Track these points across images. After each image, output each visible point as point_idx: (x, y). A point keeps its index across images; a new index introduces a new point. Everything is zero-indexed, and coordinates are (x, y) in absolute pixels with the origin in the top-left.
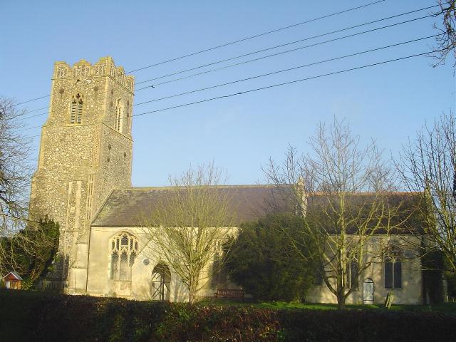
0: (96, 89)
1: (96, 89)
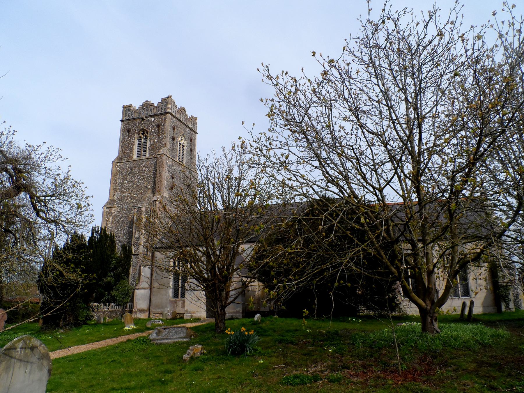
0: (158, 126)
1: (158, 126)
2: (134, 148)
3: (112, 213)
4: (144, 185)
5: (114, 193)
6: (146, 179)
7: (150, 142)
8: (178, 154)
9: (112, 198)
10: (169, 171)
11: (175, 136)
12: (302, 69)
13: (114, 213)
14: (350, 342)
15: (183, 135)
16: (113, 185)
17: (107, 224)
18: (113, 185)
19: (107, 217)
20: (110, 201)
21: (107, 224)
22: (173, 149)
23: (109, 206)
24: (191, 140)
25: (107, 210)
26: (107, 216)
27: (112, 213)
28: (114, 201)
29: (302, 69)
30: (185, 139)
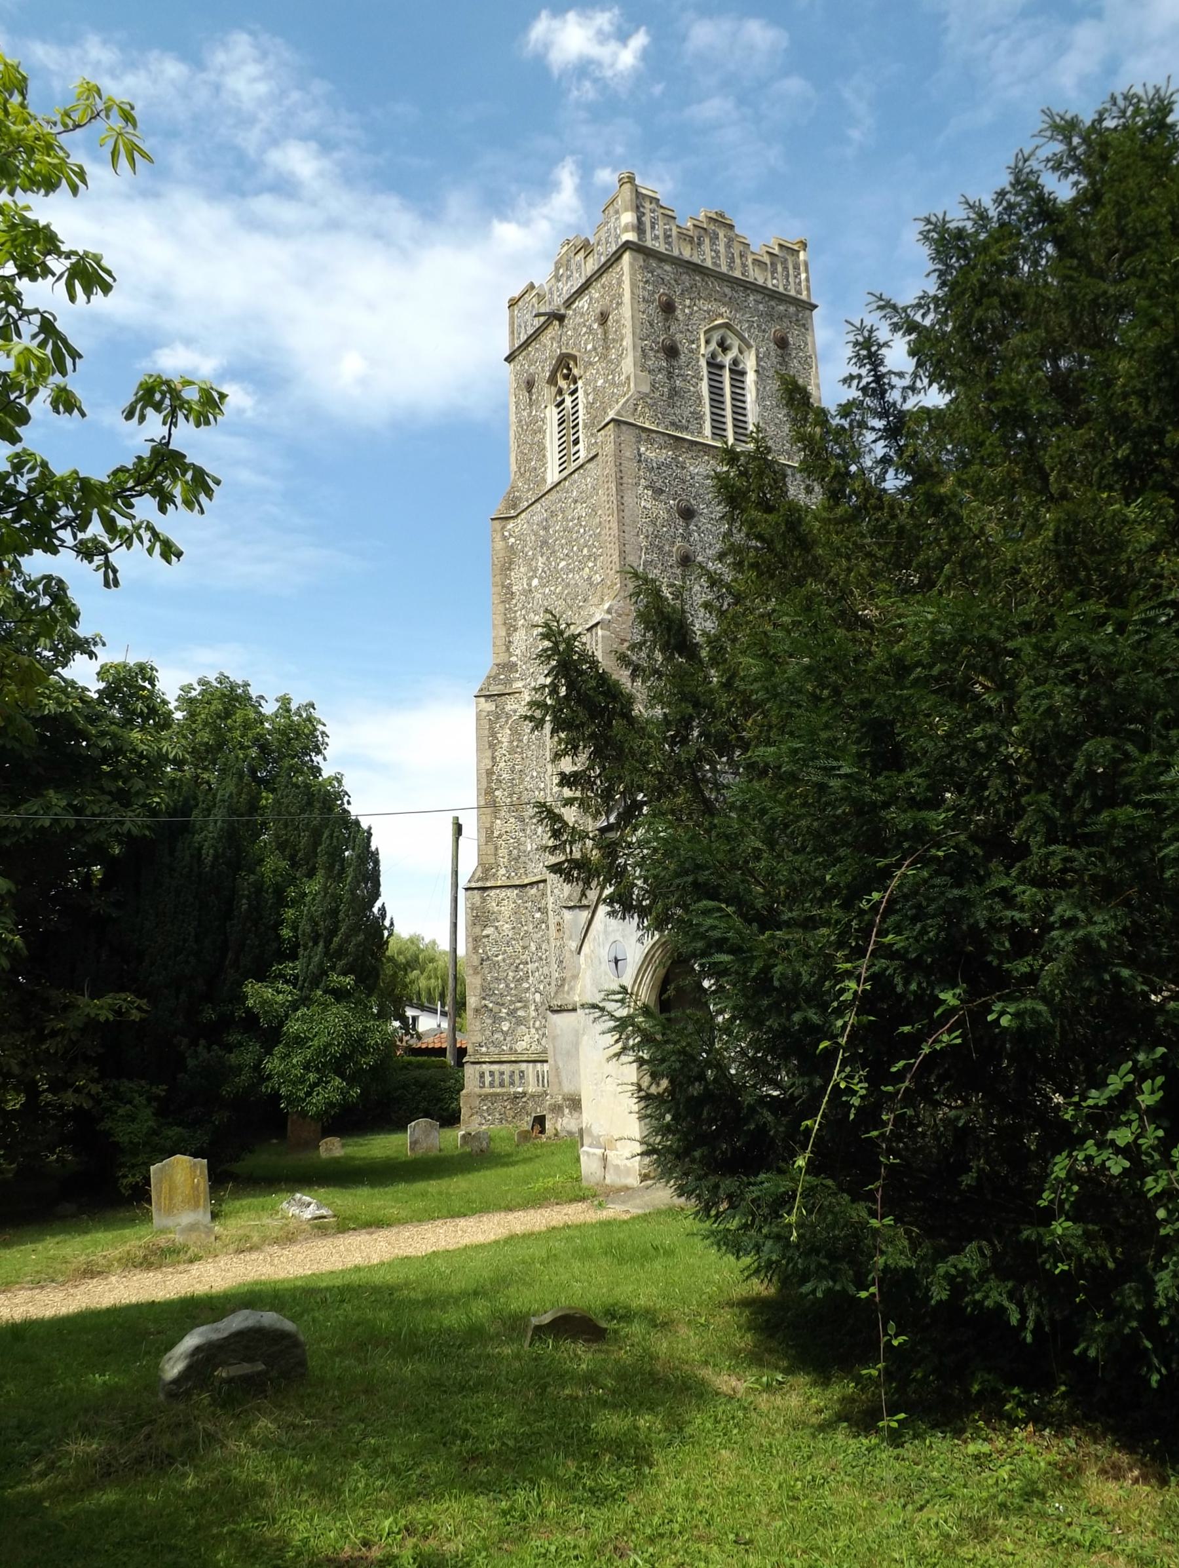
2: (548, 445)
3: (508, 717)
4: (581, 577)
5: (509, 635)
6: (585, 551)
7: (587, 394)
8: (707, 409)
9: (502, 658)
10: (658, 492)
11: (678, 336)
12: (1169, 77)
13: (515, 711)
14: (1054, 331)
15: (726, 326)
16: (501, 608)
17: (494, 758)
18: (501, 608)
19: (494, 734)
20: (495, 670)
21: (494, 758)
22: (674, 392)
23: (495, 690)
24: (782, 343)
25: (489, 706)
26: (491, 728)
27: (508, 717)
28: (512, 667)
29: (1169, 77)
30: (742, 339)
